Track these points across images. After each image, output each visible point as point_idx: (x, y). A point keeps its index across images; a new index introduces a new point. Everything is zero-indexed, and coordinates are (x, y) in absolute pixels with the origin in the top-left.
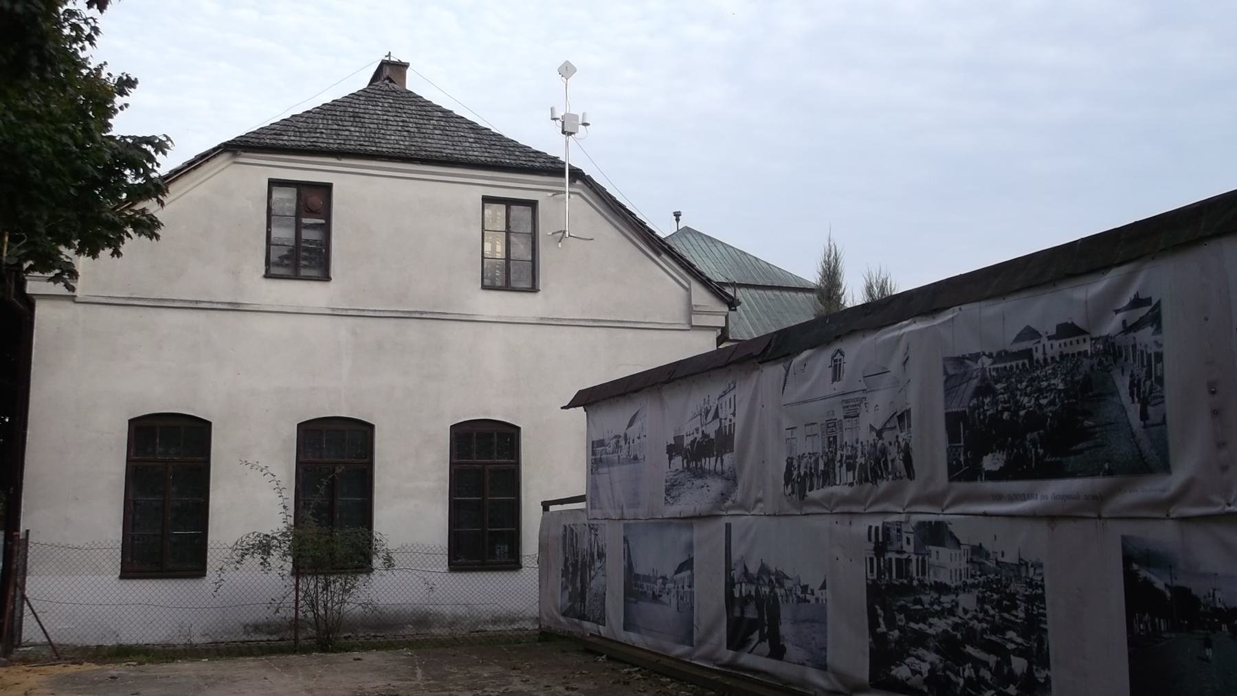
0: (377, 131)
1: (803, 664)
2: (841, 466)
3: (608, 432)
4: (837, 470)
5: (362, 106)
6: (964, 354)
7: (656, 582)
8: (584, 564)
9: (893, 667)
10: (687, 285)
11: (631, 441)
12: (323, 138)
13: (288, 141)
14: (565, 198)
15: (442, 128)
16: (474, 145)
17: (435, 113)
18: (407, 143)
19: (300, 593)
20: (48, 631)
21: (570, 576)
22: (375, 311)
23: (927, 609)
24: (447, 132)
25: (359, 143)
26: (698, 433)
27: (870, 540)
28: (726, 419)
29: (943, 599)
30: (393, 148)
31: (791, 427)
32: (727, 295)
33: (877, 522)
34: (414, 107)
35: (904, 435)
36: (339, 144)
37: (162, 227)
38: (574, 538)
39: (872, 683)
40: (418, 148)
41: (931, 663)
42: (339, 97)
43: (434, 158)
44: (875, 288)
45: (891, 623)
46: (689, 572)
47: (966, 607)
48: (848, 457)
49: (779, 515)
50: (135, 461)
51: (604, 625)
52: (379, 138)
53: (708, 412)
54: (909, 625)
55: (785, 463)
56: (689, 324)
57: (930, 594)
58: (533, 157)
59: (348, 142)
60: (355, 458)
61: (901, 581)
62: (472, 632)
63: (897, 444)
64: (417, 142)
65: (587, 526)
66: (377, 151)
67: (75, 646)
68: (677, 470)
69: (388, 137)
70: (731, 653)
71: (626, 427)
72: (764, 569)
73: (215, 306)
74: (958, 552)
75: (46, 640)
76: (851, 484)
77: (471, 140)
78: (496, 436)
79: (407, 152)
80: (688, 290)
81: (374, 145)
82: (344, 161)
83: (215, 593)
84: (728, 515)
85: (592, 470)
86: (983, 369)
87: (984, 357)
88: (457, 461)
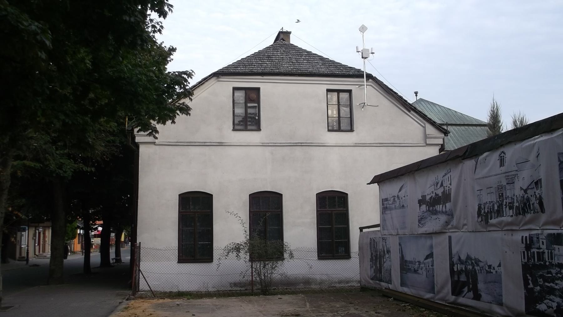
1: (491, 303)
2: (506, 207)
3: (390, 195)
4: (504, 209)
7: (415, 264)
8: (380, 256)
11: (401, 199)
12: (255, 68)
14: (364, 88)
15: (307, 59)
16: (322, 66)
17: (304, 53)
18: (292, 67)
21: (374, 261)
22: (281, 143)
24: (309, 61)
25: (271, 69)
27: (523, 243)
28: (446, 187)
31: (480, 189)
32: (443, 129)
33: (526, 234)
34: (294, 51)
35: (539, 192)
36: (262, 70)
40: (297, 69)
41: (557, 303)
42: (261, 49)
44: (518, 122)
45: (535, 283)
46: (431, 259)
48: (510, 203)
49: (475, 232)
50: (182, 212)
51: (391, 284)
53: (437, 184)
55: (478, 207)
57: (555, 269)
58: (349, 70)
59: (266, 69)
60: (274, 209)
63: (535, 196)
64: (296, 66)
65: (381, 238)
68: (423, 211)
69: (284, 65)
70: (454, 297)
72: (468, 257)
75: (149, 289)
76: (512, 216)
77: (320, 64)
79: (292, 71)
80: (424, 127)
82: (265, 77)
83: (217, 269)
84: (449, 232)
85: (382, 212)
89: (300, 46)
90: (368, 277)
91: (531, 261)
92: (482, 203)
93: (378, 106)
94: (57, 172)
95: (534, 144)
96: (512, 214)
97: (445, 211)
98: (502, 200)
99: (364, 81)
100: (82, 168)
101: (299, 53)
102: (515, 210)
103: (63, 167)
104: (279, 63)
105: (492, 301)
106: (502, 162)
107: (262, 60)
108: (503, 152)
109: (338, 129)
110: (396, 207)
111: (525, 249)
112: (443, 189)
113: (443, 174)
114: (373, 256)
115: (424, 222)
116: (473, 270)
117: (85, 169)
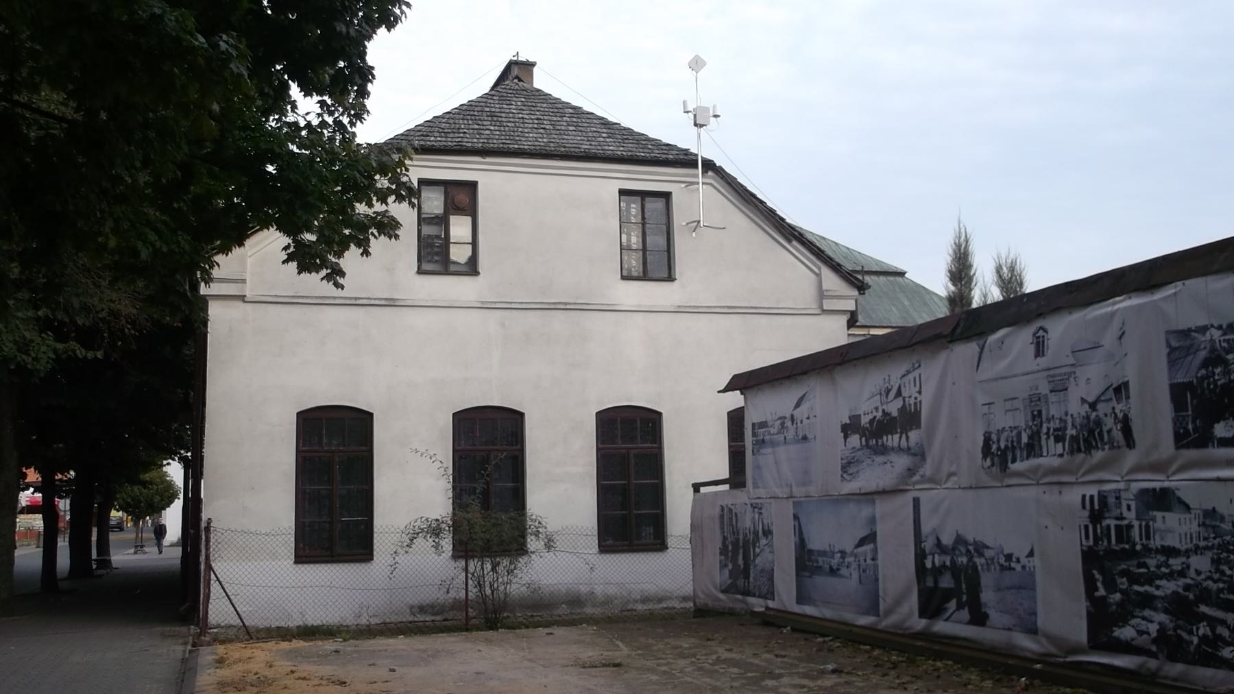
0: (515, 129)
1: (1009, 629)
2: (1048, 438)
3: (771, 414)
4: (1043, 442)
5: (497, 106)
6: (1189, 326)
8: (746, 542)
9: (1114, 629)
10: (817, 271)
11: (799, 422)
12: (467, 138)
13: (435, 141)
14: (698, 189)
15: (575, 124)
16: (608, 140)
17: (566, 110)
18: (545, 140)
19: (469, 575)
20: (240, 613)
21: (730, 554)
22: (522, 303)
23: (1153, 572)
24: (580, 128)
25: (500, 141)
26: (877, 412)
27: (1084, 507)
28: (910, 397)
29: (1171, 561)
30: (534, 146)
31: (988, 402)
32: (857, 279)
33: (1093, 491)
34: (545, 105)
35: (1123, 406)
36: (483, 143)
37: (401, 228)
38: (734, 518)
39: (1091, 645)
40: (556, 145)
41: (1160, 624)
42: (473, 97)
43: (573, 154)
44: (1005, 269)
45: (1111, 586)
46: (872, 546)
47: (1198, 568)
48: (1055, 430)
50: (304, 451)
51: (774, 600)
52: (518, 136)
53: (888, 391)
54: (1132, 588)
55: (982, 438)
56: (820, 308)
57: (1156, 557)
58: (666, 150)
59: (491, 141)
60: (507, 445)
61: (1122, 546)
62: (624, 611)
63: (1113, 415)
64: (554, 138)
65: (749, 506)
66: (519, 148)
67: (258, 627)
68: (854, 448)
69: (527, 135)
70: (924, 622)
71: (792, 408)
72: (960, 540)
73: (373, 302)
74: (1188, 516)
75: (241, 624)
76: (1061, 455)
77: (604, 135)
78: (639, 423)
79: (548, 148)
80: (818, 275)
81: (515, 142)
82: (488, 160)
83: (390, 576)
84: (916, 490)
85: (753, 451)
86: (1212, 341)
87: (1213, 329)
88: (602, 446)
89: (555, 95)
90: (715, 587)
91: (1102, 544)
92: (993, 429)
93: (724, 228)
94: (19, 359)
95: (1113, 314)
96: (1061, 452)
97: (906, 447)
98: (1039, 425)
99: (698, 175)
100: (74, 351)
101: (556, 110)
102: (1069, 445)
103: (31, 348)
104: (515, 129)
105: (1013, 626)
106: (1040, 348)
107: (480, 123)
108: (1041, 328)
109: (641, 275)
110: (787, 441)
111: (1088, 520)
112: (902, 403)
113: (903, 370)
114: (727, 543)
115: (856, 470)
116: (971, 564)
117: (81, 354)
